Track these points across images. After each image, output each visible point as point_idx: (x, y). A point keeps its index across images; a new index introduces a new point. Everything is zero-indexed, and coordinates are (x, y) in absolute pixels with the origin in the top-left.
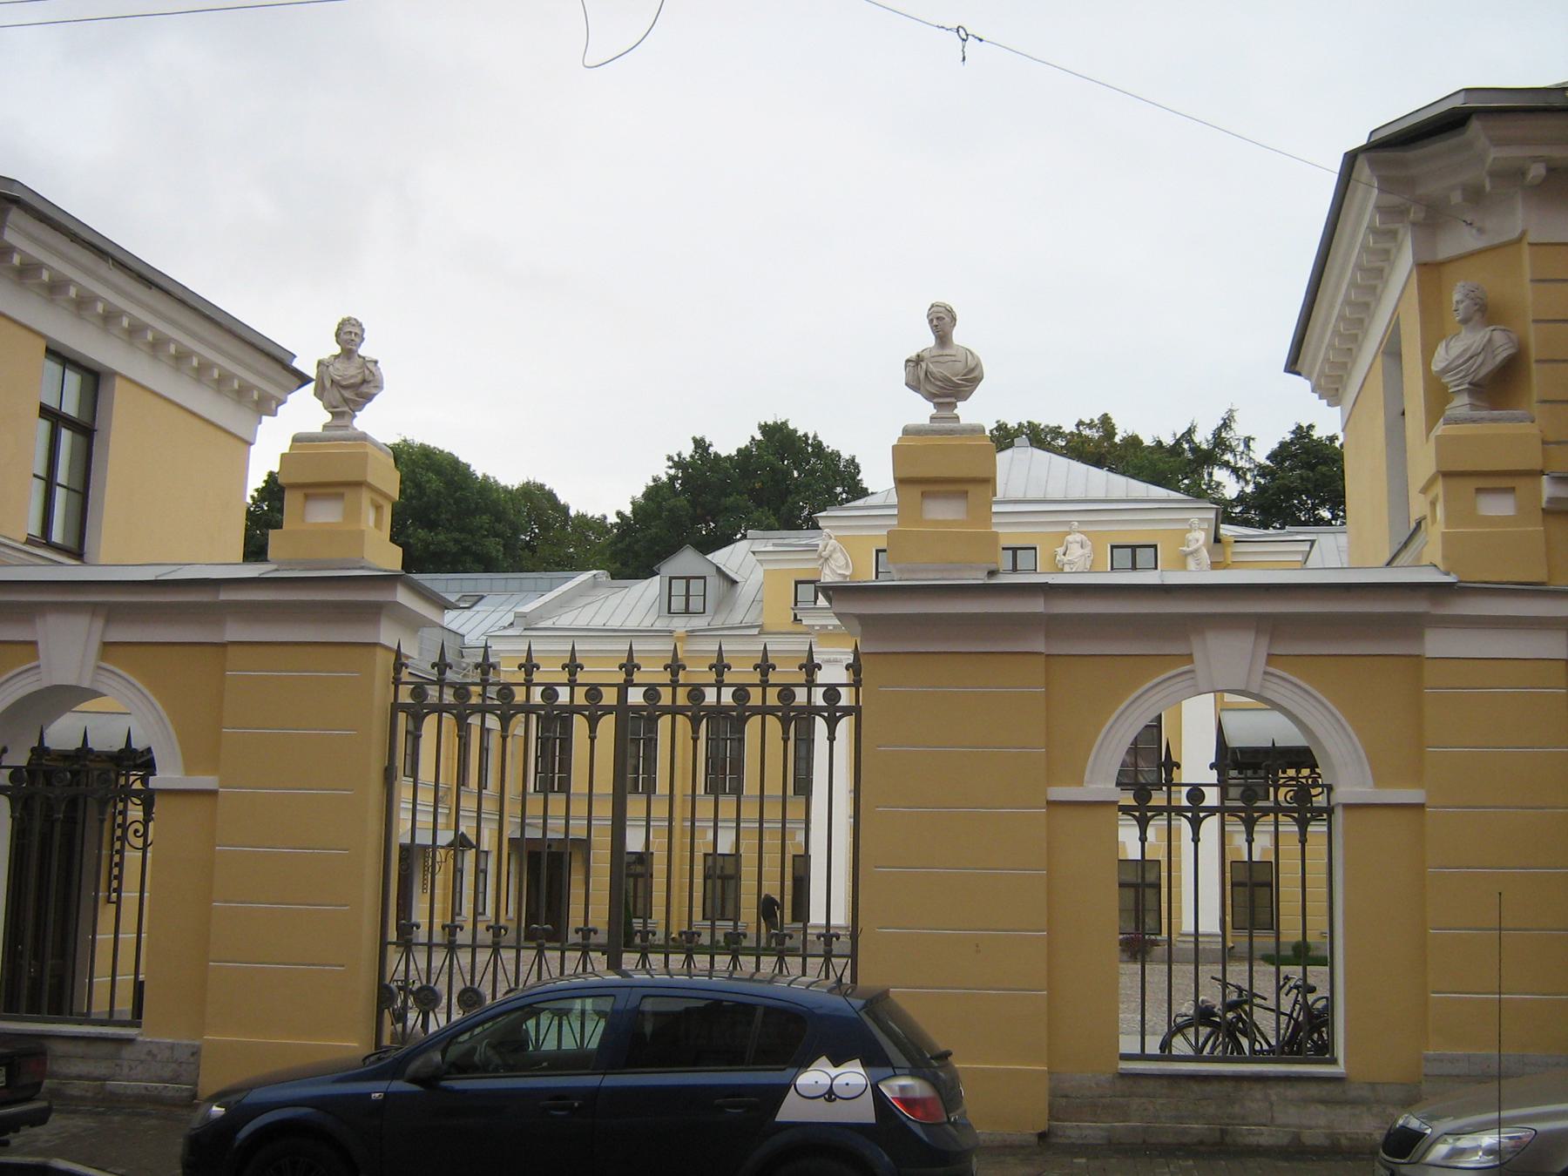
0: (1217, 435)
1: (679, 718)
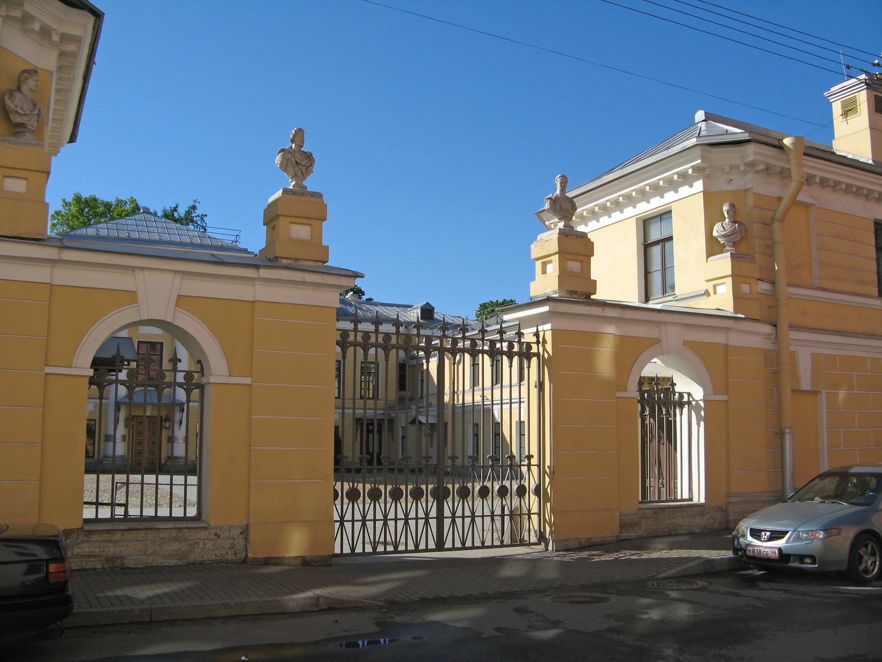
0: (188, 213)
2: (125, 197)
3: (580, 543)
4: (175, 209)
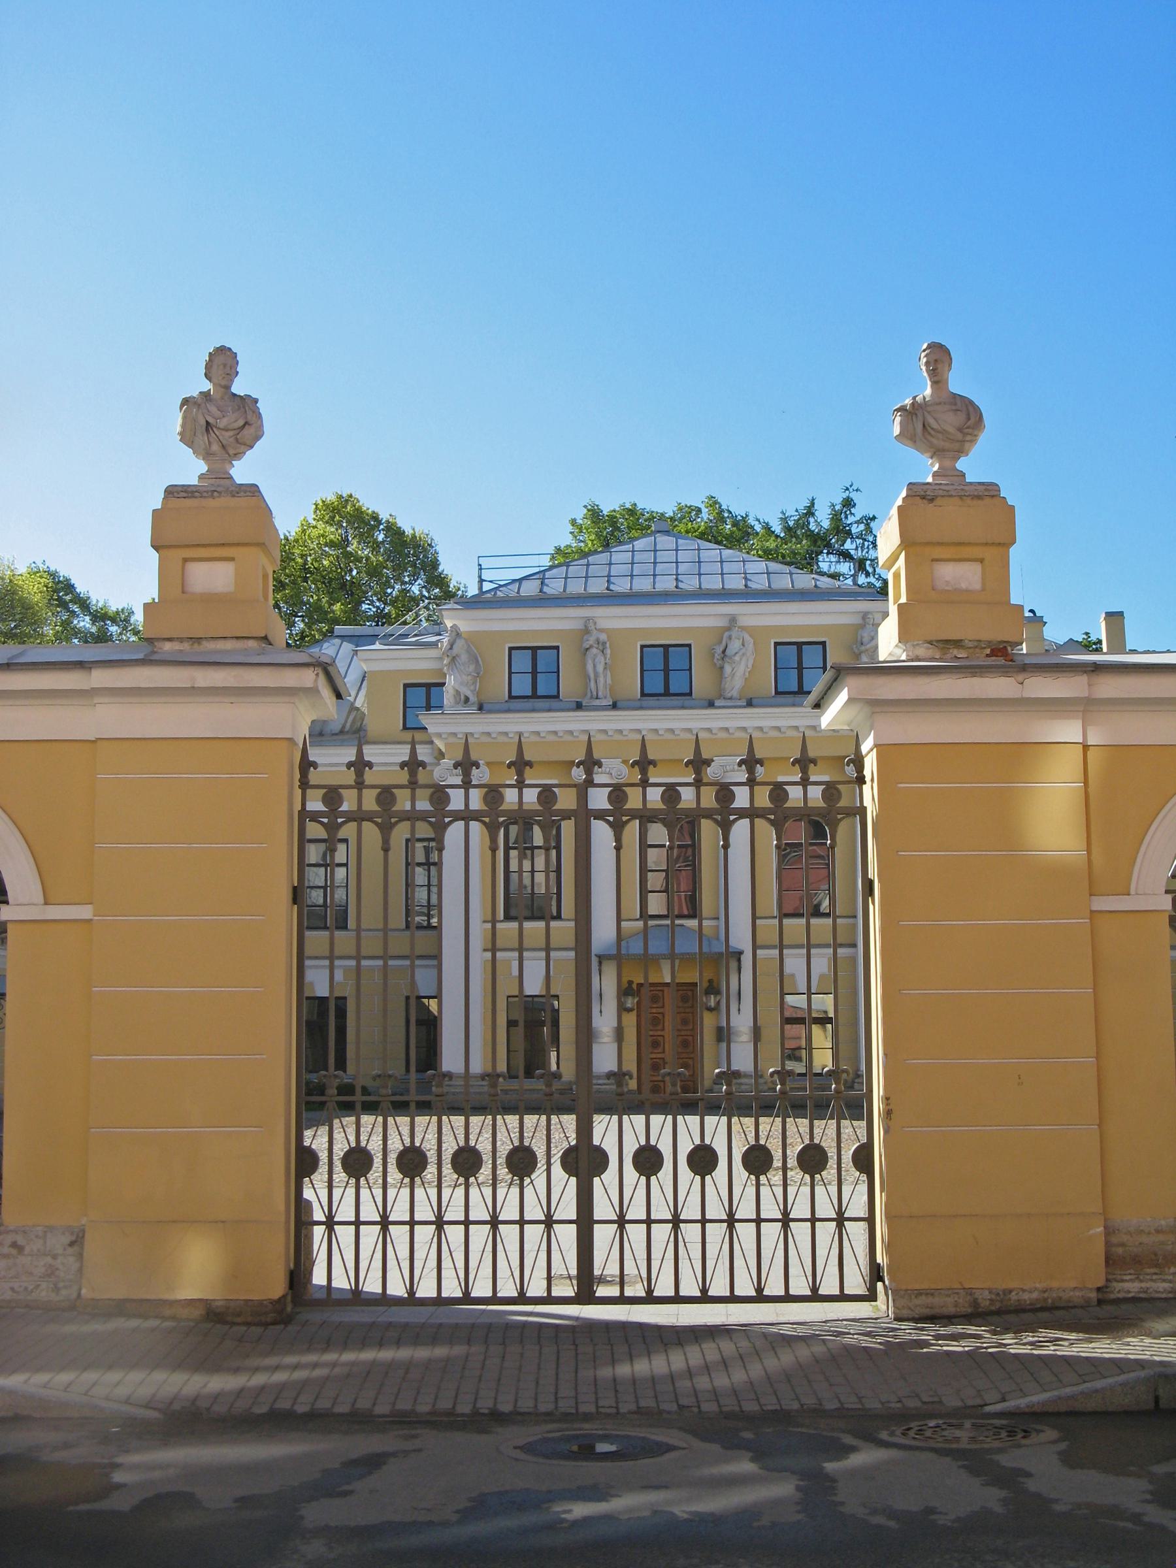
0: (836, 517)
1: (366, 825)
2: (697, 499)
3: (975, 1303)
4: (810, 512)
